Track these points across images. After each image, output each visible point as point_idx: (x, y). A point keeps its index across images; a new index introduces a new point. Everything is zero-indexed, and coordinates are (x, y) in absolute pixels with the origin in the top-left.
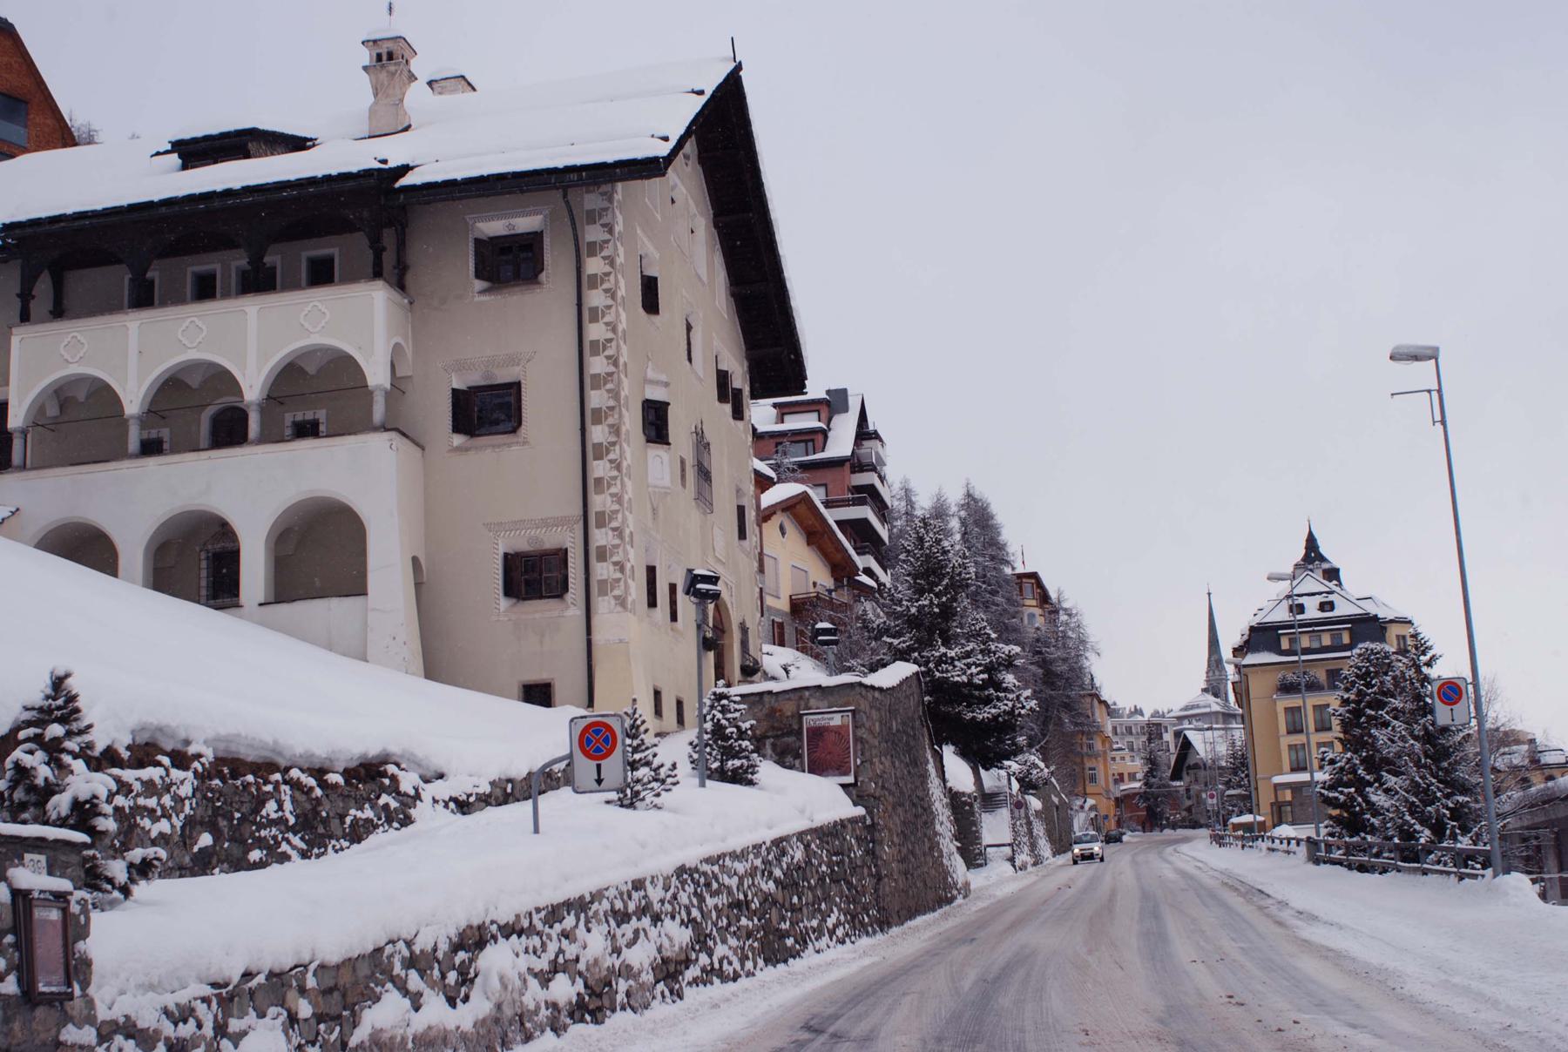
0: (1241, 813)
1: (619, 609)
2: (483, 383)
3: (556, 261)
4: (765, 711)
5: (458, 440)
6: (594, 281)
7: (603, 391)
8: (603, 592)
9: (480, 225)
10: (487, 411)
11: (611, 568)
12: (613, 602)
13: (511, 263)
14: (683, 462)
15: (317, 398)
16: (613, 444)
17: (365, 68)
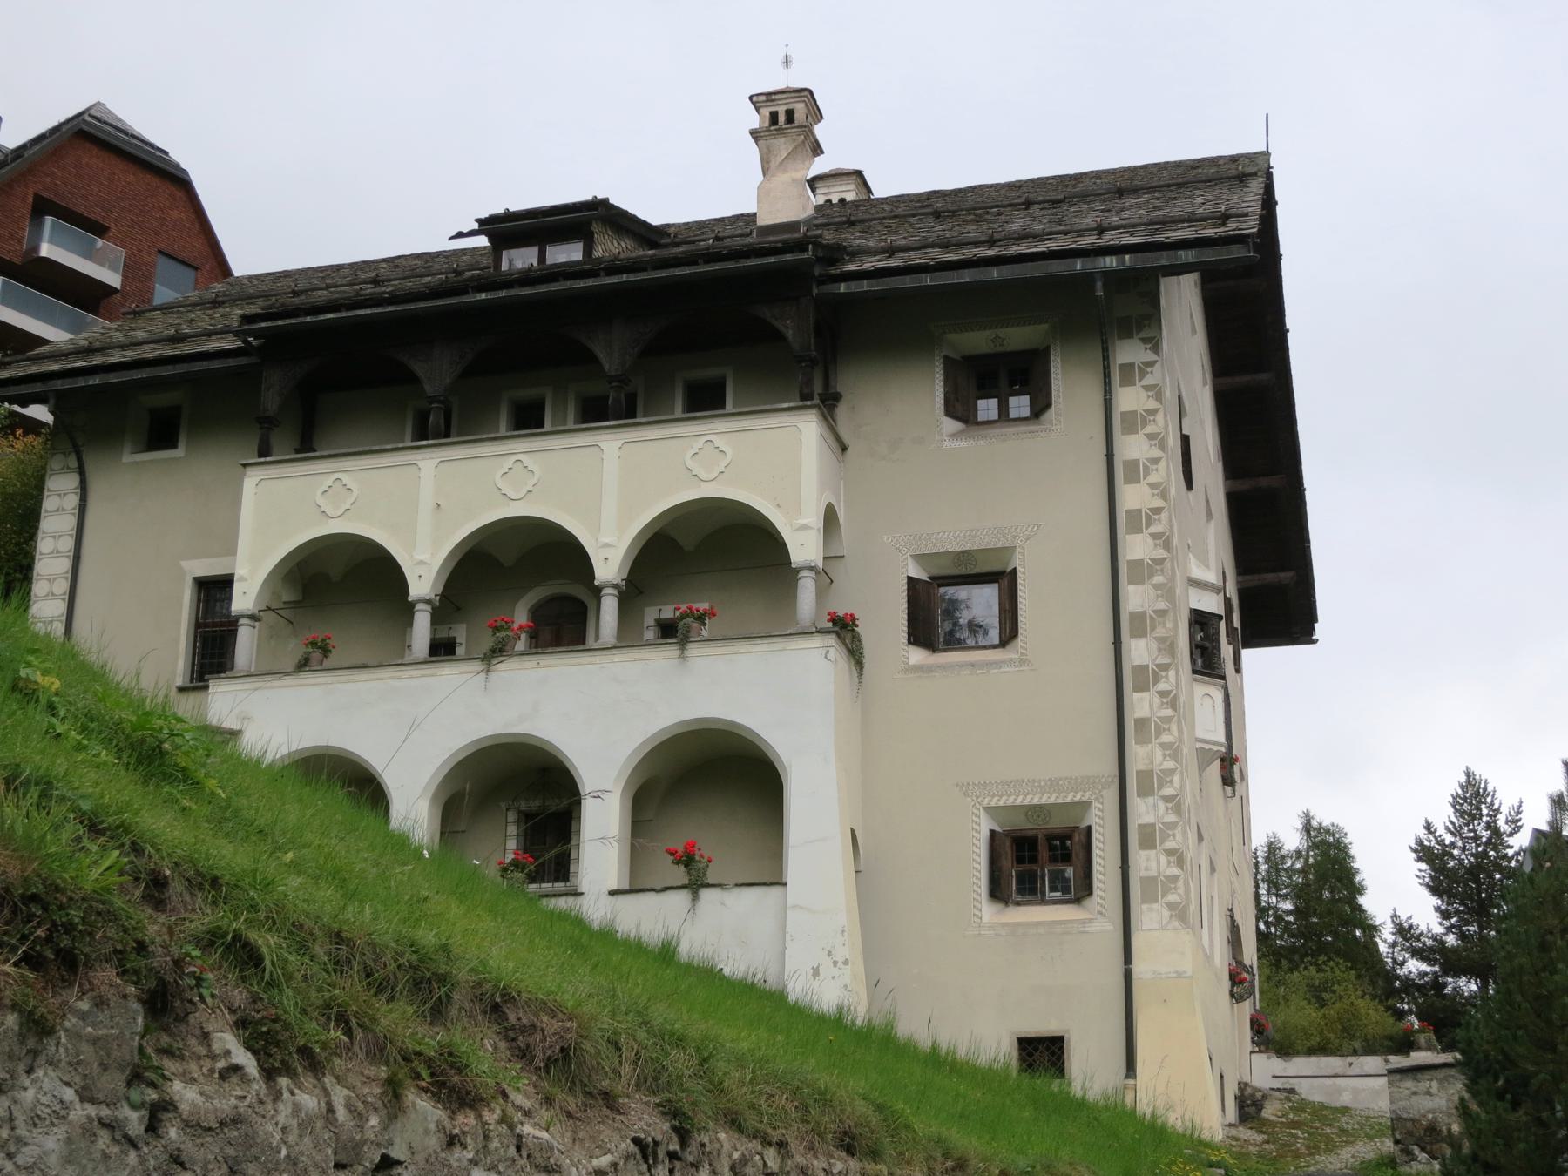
5: (917, 656)
12: (1166, 913)
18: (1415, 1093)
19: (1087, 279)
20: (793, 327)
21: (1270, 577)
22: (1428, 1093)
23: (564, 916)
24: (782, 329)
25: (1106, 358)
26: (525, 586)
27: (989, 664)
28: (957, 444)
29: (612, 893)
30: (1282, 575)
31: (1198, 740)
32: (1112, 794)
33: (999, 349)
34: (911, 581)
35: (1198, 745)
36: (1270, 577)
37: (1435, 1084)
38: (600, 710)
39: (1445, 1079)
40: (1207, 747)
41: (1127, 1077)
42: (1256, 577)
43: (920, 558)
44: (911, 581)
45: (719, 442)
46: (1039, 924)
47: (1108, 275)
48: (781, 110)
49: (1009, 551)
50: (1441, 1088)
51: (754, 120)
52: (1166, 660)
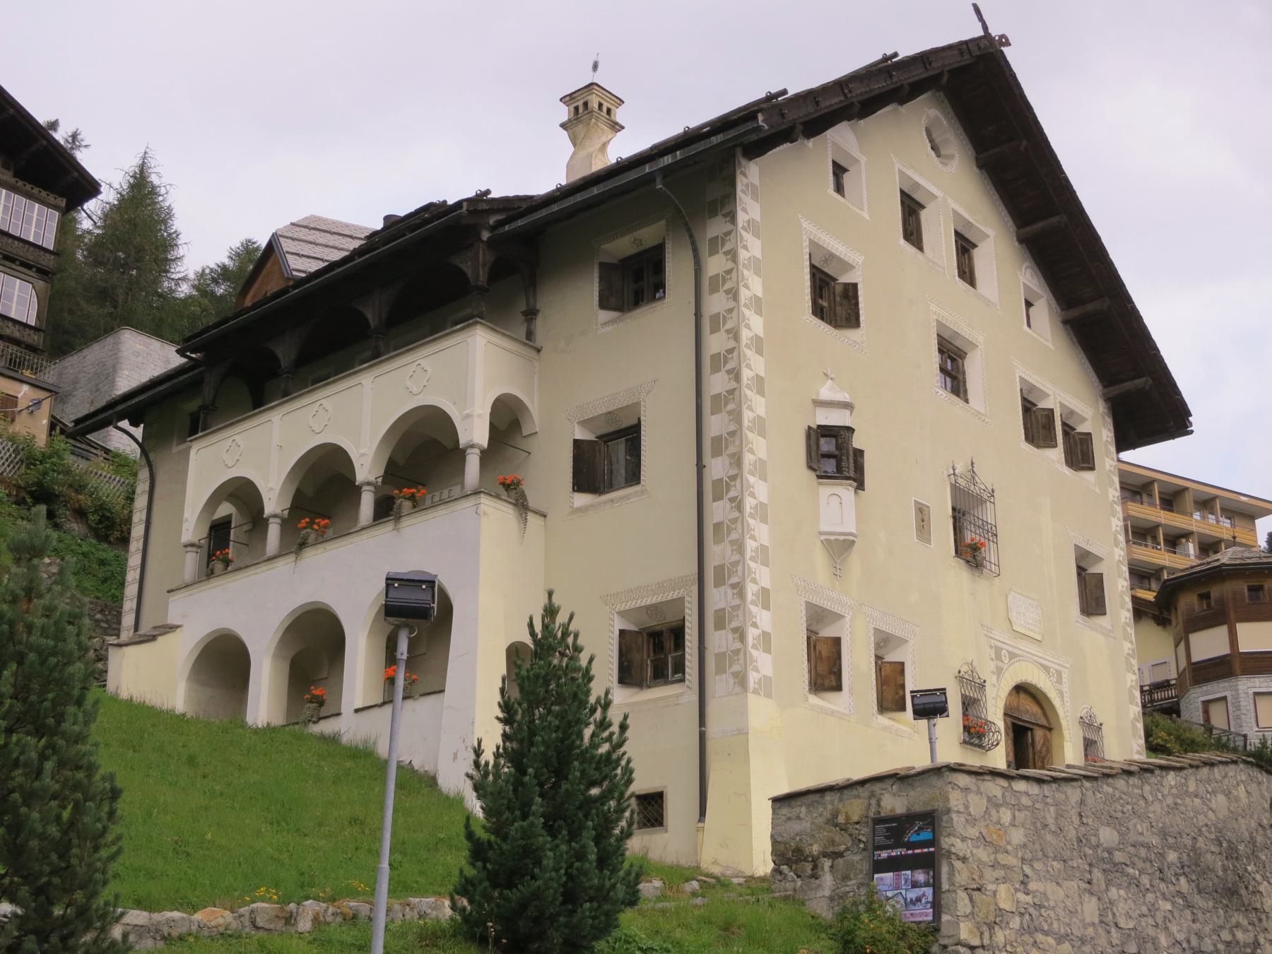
0: (171, 910)
1: (738, 689)
2: (611, 429)
3: (677, 270)
4: (827, 814)
5: (582, 499)
6: (716, 284)
7: (724, 413)
8: (720, 670)
9: (606, 246)
10: (608, 459)
11: (730, 636)
12: (731, 681)
13: (635, 284)
14: (922, 512)
15: (424, 459)
16: (733, 478)
17: (563, 126)
18: (789, 819)
19: (649, 179)
20: (476, 265)
21: (1128, 385)
22: (798, 818)
23: (323, 738)
24: (465, 269)
25: (691, 237)
26: (325, 492)
27: (622, 498)
28: (609, 328)
29: (357, 711)
30: (1137, 381)
31: (821, 533)
32: (695, 588)
33: (642, 248)
34: (577, 443)
35: (823, 538)
36: (1128, 385)
37: (803, 809)
38: (348, 575)
39: (812, 804)
40: (832, 538)
41: (700, 821)
42: (1117, 387)
43: (583, 423)
44: (577, 443)
45: (424, 363)
46: (666, 697)
47: (666, 171)
48: (580, 103)
49: (636, 407)
50: (809, 812)
51: (564, 113)
52: (735, 472)
